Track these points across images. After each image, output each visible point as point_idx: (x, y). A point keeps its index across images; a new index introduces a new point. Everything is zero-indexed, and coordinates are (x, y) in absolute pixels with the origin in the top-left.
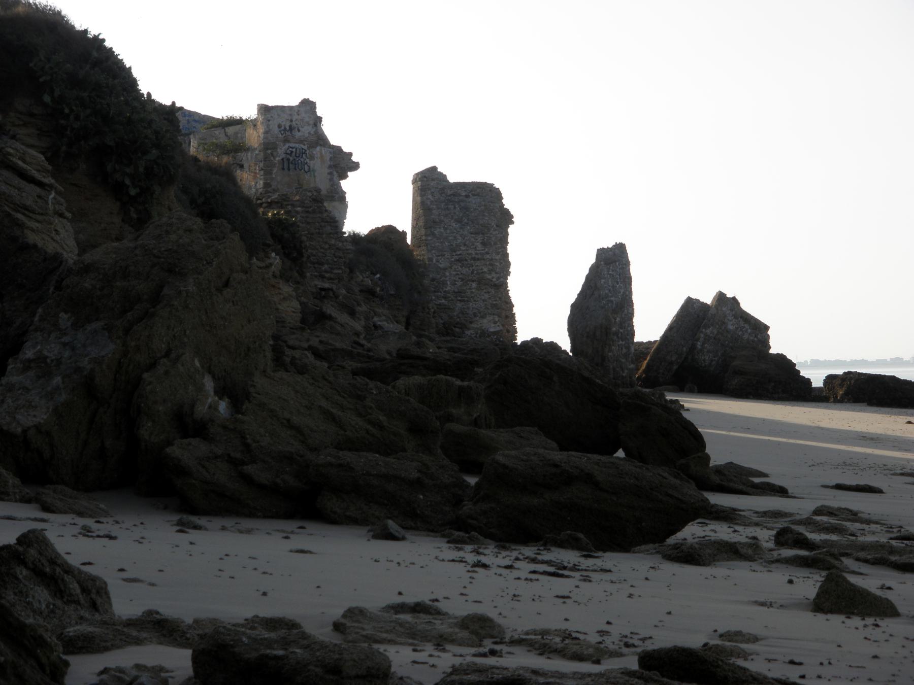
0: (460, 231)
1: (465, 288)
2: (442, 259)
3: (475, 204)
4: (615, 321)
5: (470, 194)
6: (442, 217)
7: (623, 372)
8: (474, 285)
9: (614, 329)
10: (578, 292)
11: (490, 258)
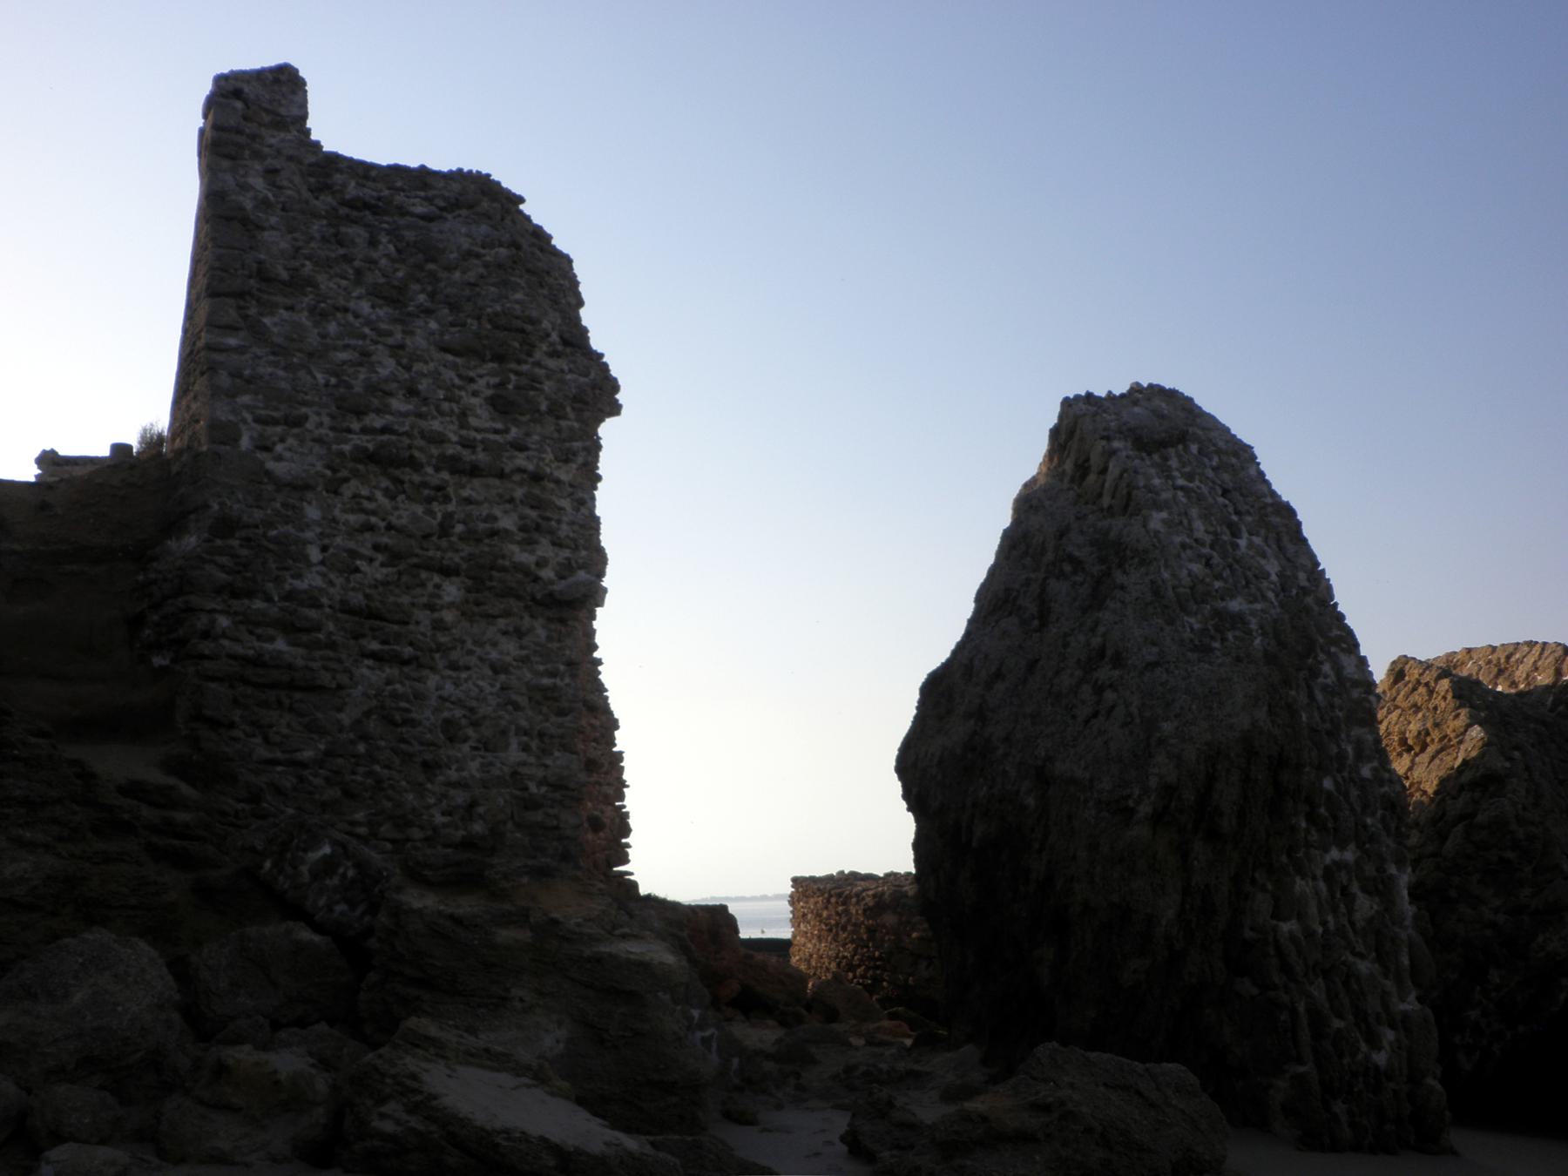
0: (390, 334)
1: (405, 600)
2: (291, 441)
7: (1374, 1042)
8: (452, 591)
11: (531, 467)
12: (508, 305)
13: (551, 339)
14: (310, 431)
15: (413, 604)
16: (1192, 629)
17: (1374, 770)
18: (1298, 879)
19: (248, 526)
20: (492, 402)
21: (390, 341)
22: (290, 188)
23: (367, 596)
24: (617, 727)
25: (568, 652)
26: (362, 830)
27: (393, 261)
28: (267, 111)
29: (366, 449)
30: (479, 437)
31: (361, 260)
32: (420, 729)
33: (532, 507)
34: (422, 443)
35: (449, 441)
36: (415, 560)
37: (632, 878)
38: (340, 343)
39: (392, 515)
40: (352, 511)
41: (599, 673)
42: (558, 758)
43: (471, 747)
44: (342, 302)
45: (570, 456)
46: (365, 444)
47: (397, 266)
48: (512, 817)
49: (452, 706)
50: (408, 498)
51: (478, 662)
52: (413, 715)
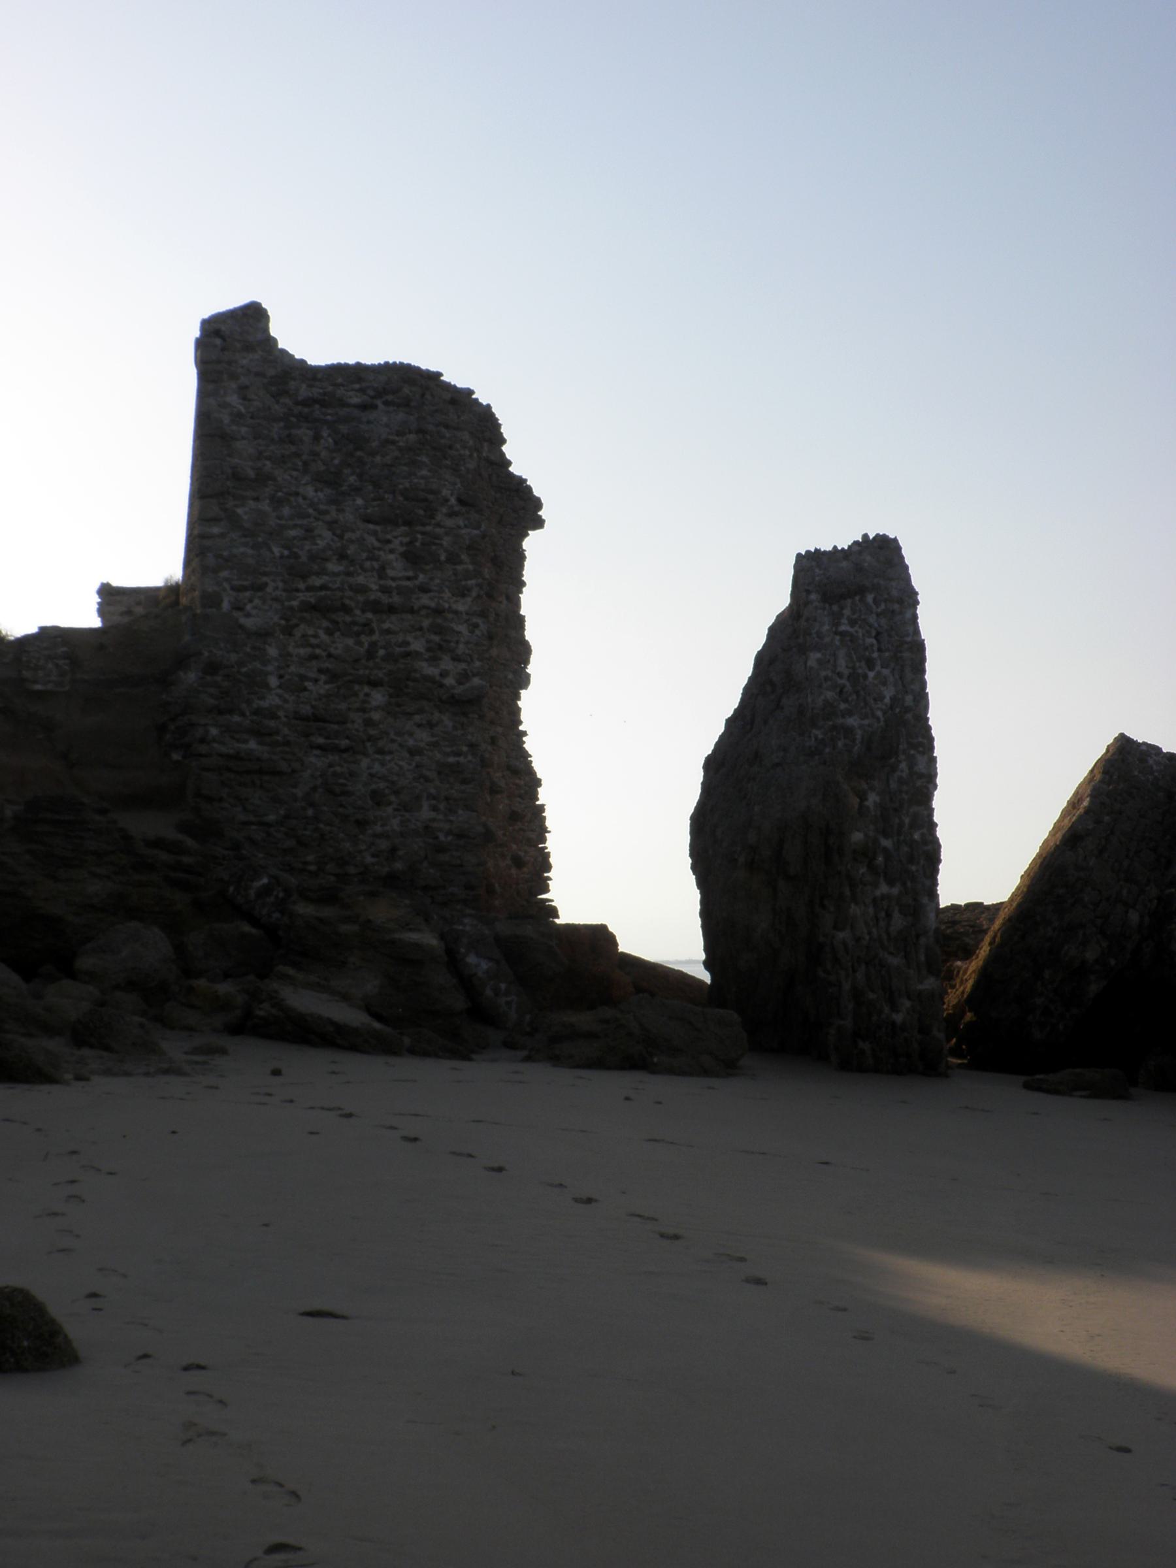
0: (327, 512)
1: (343, 706)
2: (257, 601)
3: (387, 425)
4: (861, 806)
5: (379, 402)
6: (268, 463)
7: (894, 1008)
8: (378, 697)
9: (857, 837)
10: (730, 713)
11: (433, 605)
12: (416, 481)
13: (449, 503)
16: (816, 739)
17: (923, 835)
18: (853, 906)
21: (328, 518)
23: (313, 707)
26: (313, 868)
30: (394, 584)
33: (435, 633)
35: (371, 590)
37: (553, 904)
38: (291, 523)
41: (524, 742)
45: (466, 592)
50: (343, 635)
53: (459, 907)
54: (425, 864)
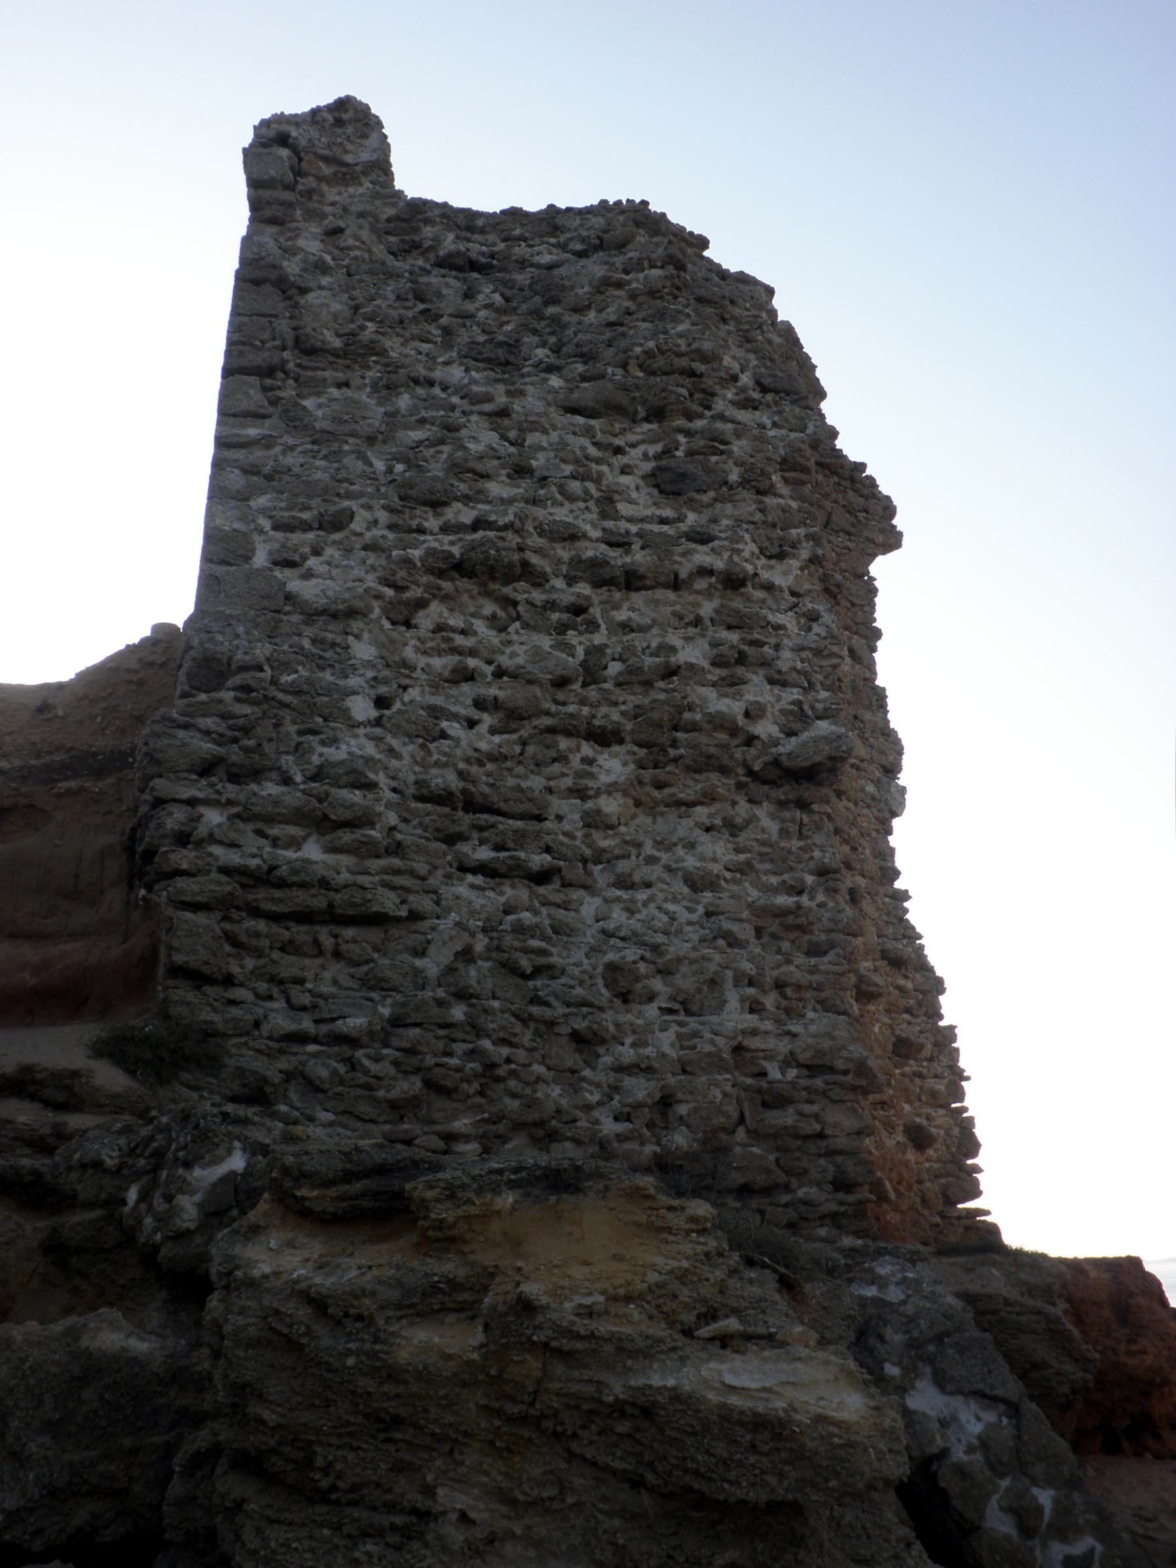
1: (536, 783)
11: (719, 564)
14: (360, 534)
15: (550, 791)
19: (243, 668)
20: (654, 479)
21: (488, 407)
22: (357, 248)
23: (461, 775)
24: (942, 991)
25: (817, 854)
27: (500, 311)
28: (327, 160)
29: (450, 555)
30: (634, 529)
31: (451, 315)
32: (563, 980)
33: (729, 627)
34: (541, 542)
36: (546, 721)
37: (988, 1219)
39: (503, 653)
40: (439, 653)
41: (906, 911)
42: (812, 1020)
43: (660, 1009)
44: (421, 371)
46: (446, 548)
47: (505, 318)
48: (742, 1120)
49: (621, 944)
50: (526, 626)
51: (665, 876)
52: (553, 960)
53: (823, 1232)
54: (741, 1135)
